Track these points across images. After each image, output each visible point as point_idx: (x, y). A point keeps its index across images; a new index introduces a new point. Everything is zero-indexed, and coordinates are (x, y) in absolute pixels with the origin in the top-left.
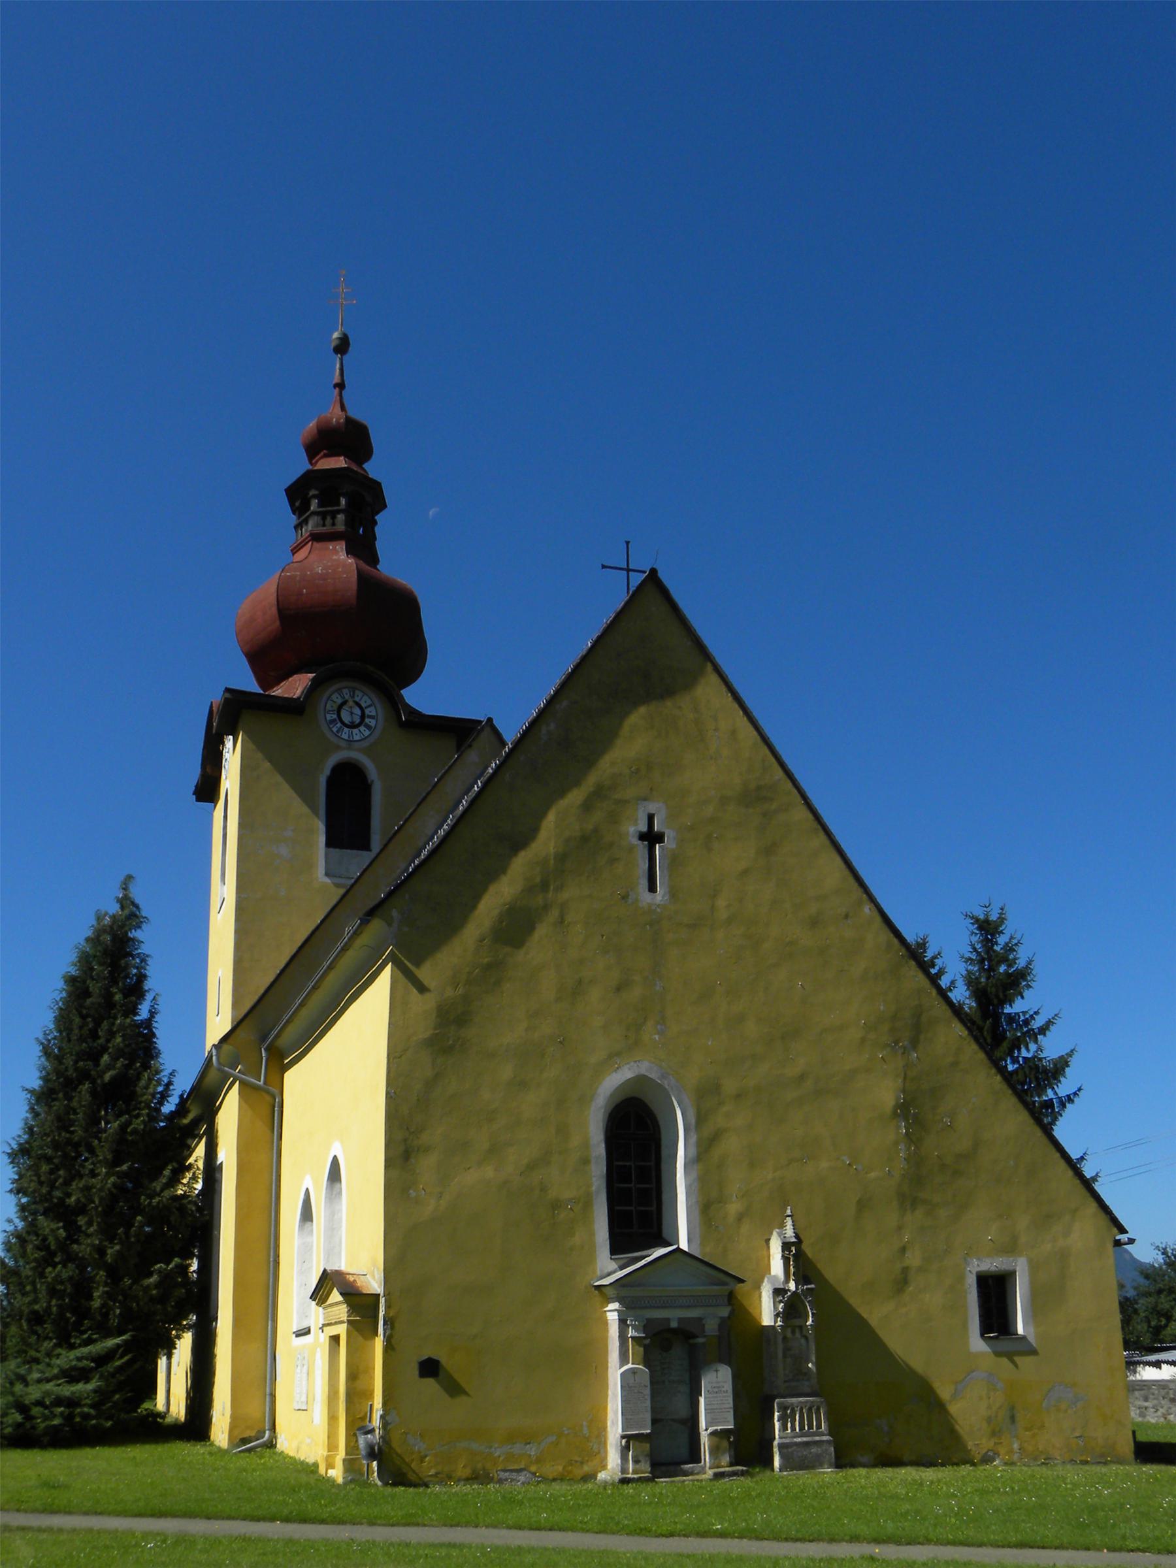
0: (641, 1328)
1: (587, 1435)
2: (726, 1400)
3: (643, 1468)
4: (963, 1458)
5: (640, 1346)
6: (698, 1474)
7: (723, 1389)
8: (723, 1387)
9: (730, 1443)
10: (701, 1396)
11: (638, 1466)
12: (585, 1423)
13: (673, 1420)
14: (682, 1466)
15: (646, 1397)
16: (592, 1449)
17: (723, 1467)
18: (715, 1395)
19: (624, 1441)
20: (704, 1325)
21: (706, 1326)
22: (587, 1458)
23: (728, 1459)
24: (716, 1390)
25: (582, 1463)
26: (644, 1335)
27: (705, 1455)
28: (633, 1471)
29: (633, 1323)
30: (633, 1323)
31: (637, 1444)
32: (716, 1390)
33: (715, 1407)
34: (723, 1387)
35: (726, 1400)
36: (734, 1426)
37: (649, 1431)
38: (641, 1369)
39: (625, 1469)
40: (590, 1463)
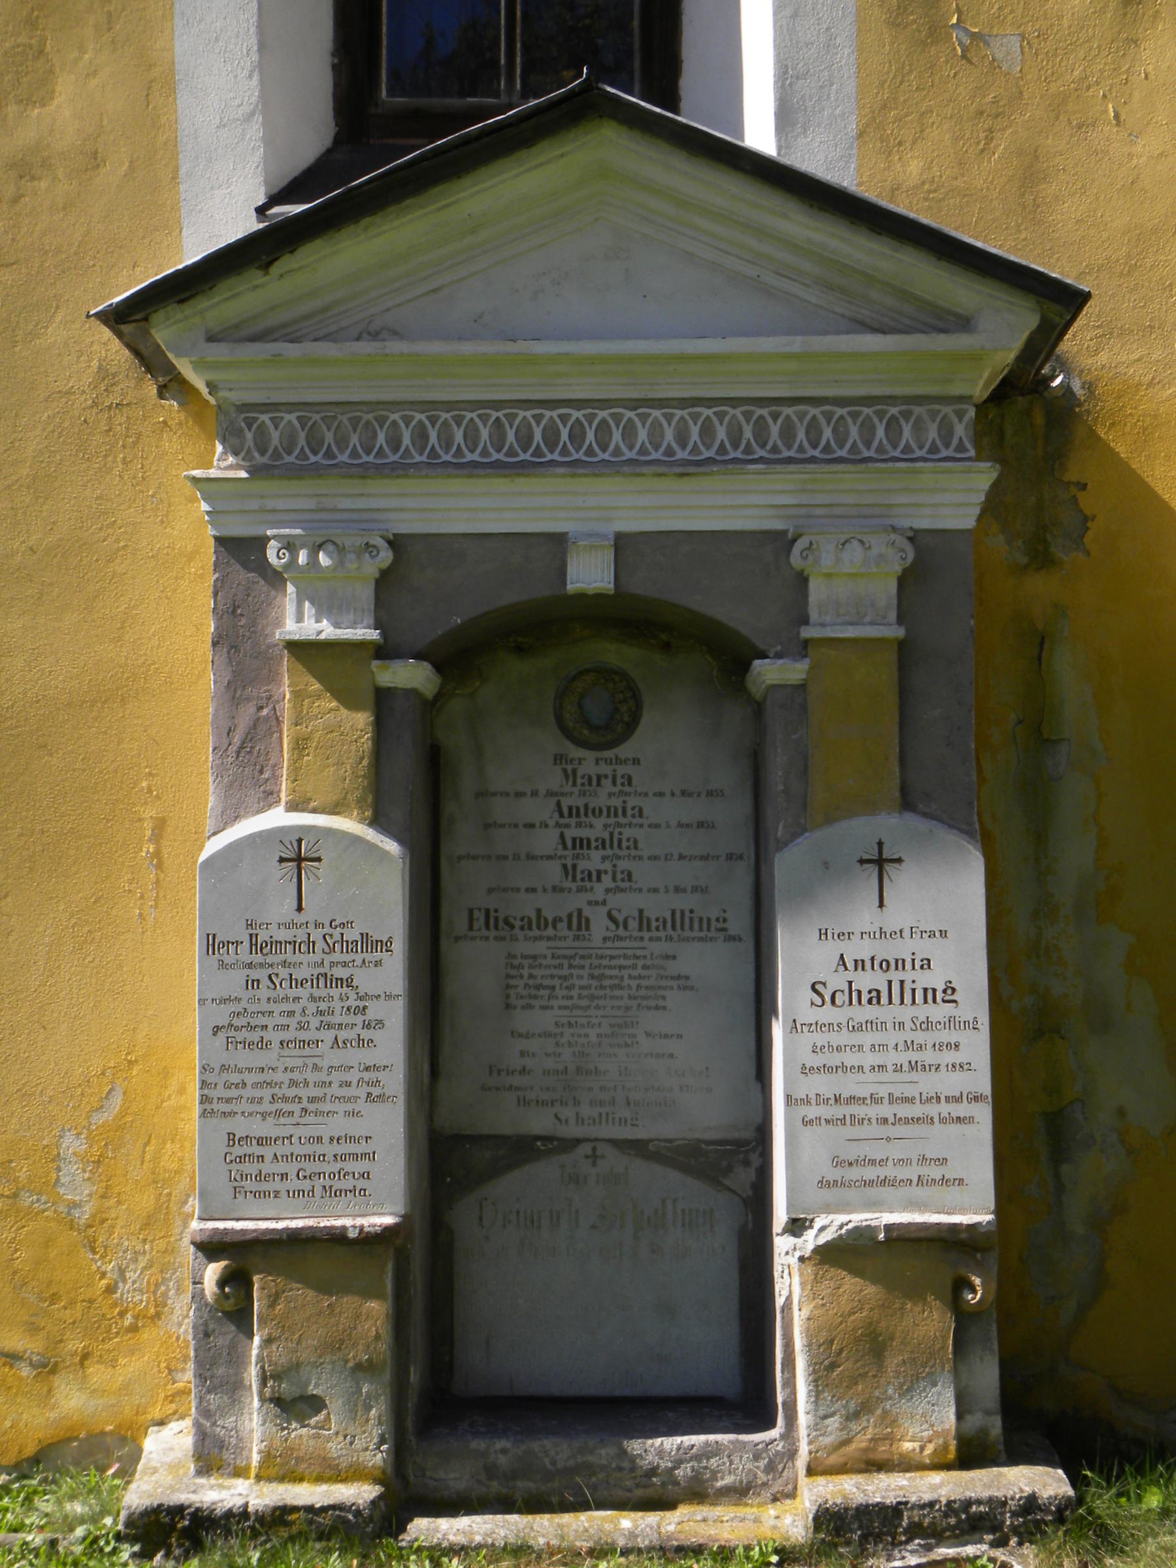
0: (366, 593)
1: (84, 1215)
2: (938, 1047)
3: (335, 1448)
4: (97, 315)
5: (348, 700)
6: (740, 1493)
7: (924, 979)
8: (927, 964)
9: (964, 1318)
10: (777, 1017)
11: (299, 1433)
12: (72, 1144)
13: (637, 1148)
14: (635, 1446)
15: (375, 1011)
16: (110, 1290)
17: (907, 1465)
18: (868, 1012)
19: (213, 1271)
20: (802, 580)
21: (817, 590)
22: (75, 1344)
23: (948, 1418)
24: (866, 981)
25: (47, 1368)
26: (374, 635)
27: (790, 1383)
28: (268, 1457)
29: (302, 557)
30: (302, 557)
31: (300, 1294)
32: (866, 981)
33: (850, 1085)
34: (927, 964)
35: (938, 1047)
36: (999, 1211)
37: (389, 1220)
38: (356, 840)
39: (221, 1445)
40: (97, 1373)
